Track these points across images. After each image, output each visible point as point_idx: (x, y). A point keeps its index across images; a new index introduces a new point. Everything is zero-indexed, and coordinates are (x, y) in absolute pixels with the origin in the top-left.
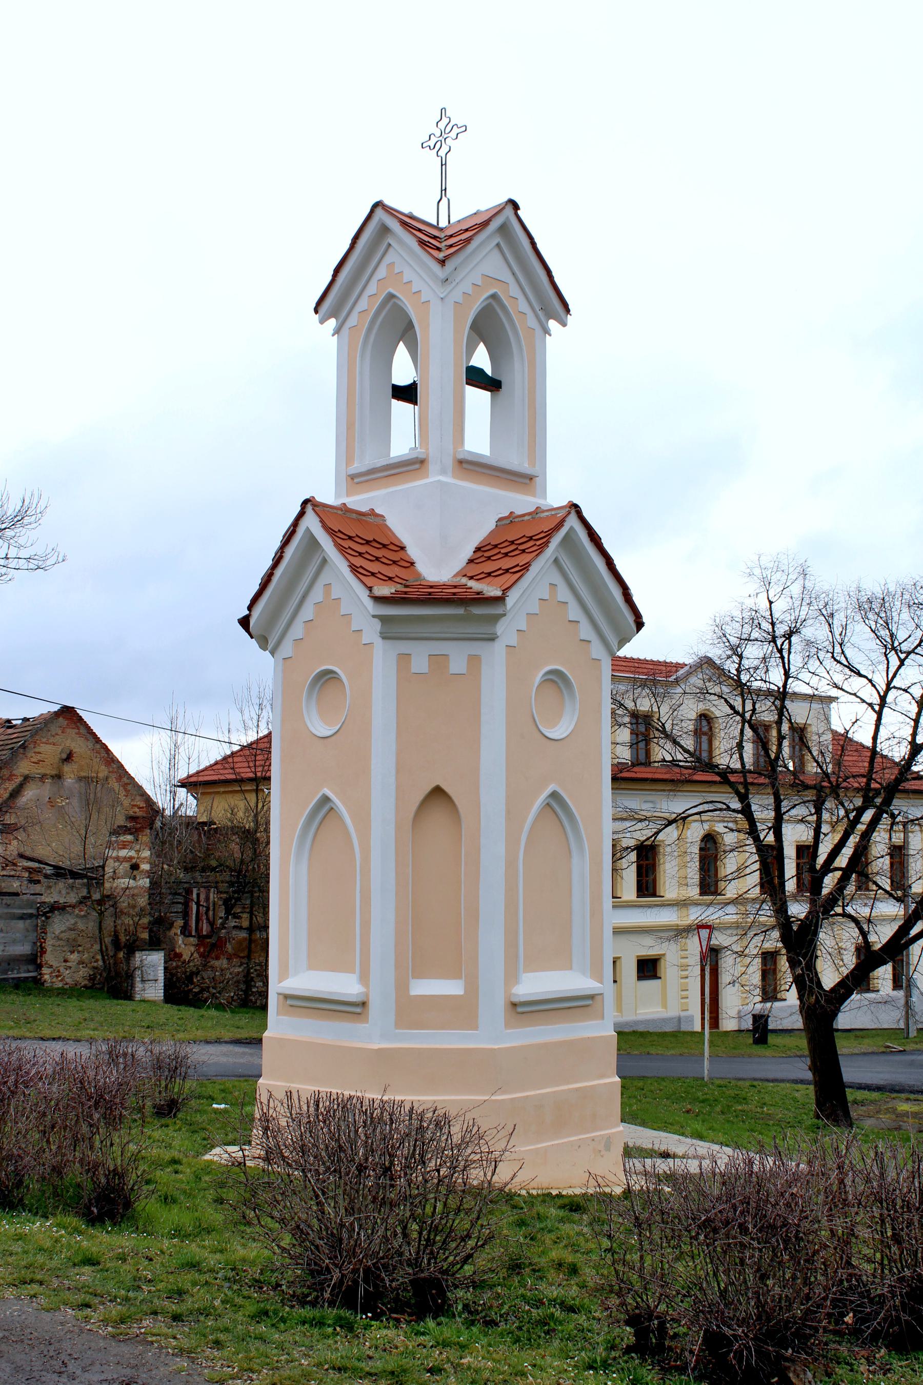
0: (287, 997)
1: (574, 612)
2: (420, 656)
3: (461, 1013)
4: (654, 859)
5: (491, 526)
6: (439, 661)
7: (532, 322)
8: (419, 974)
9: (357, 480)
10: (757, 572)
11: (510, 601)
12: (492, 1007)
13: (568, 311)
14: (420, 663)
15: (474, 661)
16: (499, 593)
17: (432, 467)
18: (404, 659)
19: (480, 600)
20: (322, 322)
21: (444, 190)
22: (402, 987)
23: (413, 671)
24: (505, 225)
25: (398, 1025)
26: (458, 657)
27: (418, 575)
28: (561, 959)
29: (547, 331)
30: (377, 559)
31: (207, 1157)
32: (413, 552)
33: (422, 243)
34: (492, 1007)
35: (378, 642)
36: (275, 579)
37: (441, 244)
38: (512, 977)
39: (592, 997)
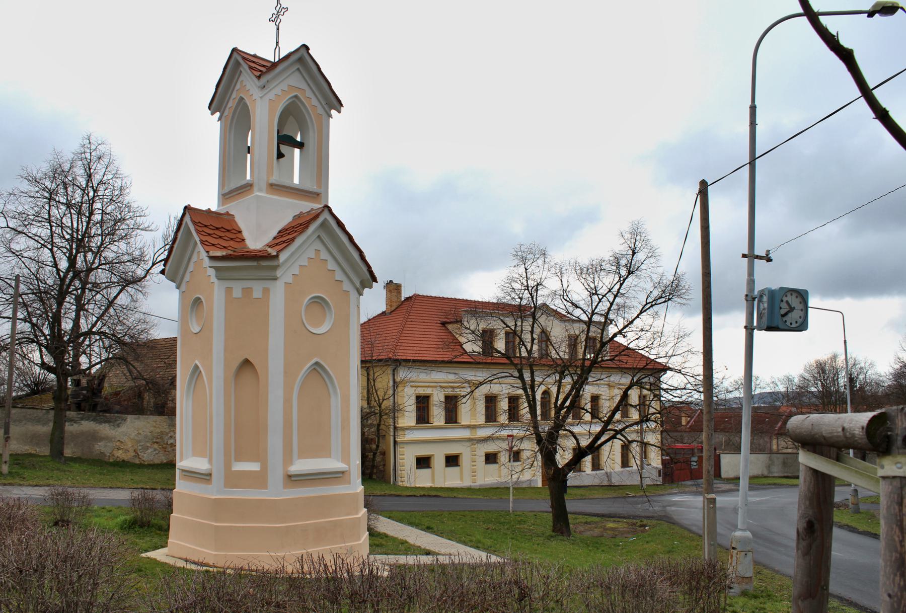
0: (183, 471)
1: (331, 265)
2: (237, 289)
3: (259, 480)
4: (428, 404)
5: (290, 219)
6: (247, 291)
7: (320, 110)
8: (238, 459)
9: (226, 196)
10: (520, 253)
11: (283, 257)
12: (276, 476)
13: (341, 105)
14: (237, 293)
15: (266, 291)
16: (275, 254)
17: (255, 188)
18: (229, 290)
19: (269, 257)
20: (212, 114)
21: (277, 43)
22: (228, 466)
23: (234, 296)
24: (302, 58)
25: (225, 487)
26: (257, 289)
27: (246, 245)
28: (322, 451)
29: (330, 116)
30: (220, 237)
31: (152, 554)
32: (245, 234)
33: (251, 68)
34: (276, 476)
35: (216, 280)
36: (174, 249)
37: (262, 69)
38: (288, 459)
39: (343, 472)
